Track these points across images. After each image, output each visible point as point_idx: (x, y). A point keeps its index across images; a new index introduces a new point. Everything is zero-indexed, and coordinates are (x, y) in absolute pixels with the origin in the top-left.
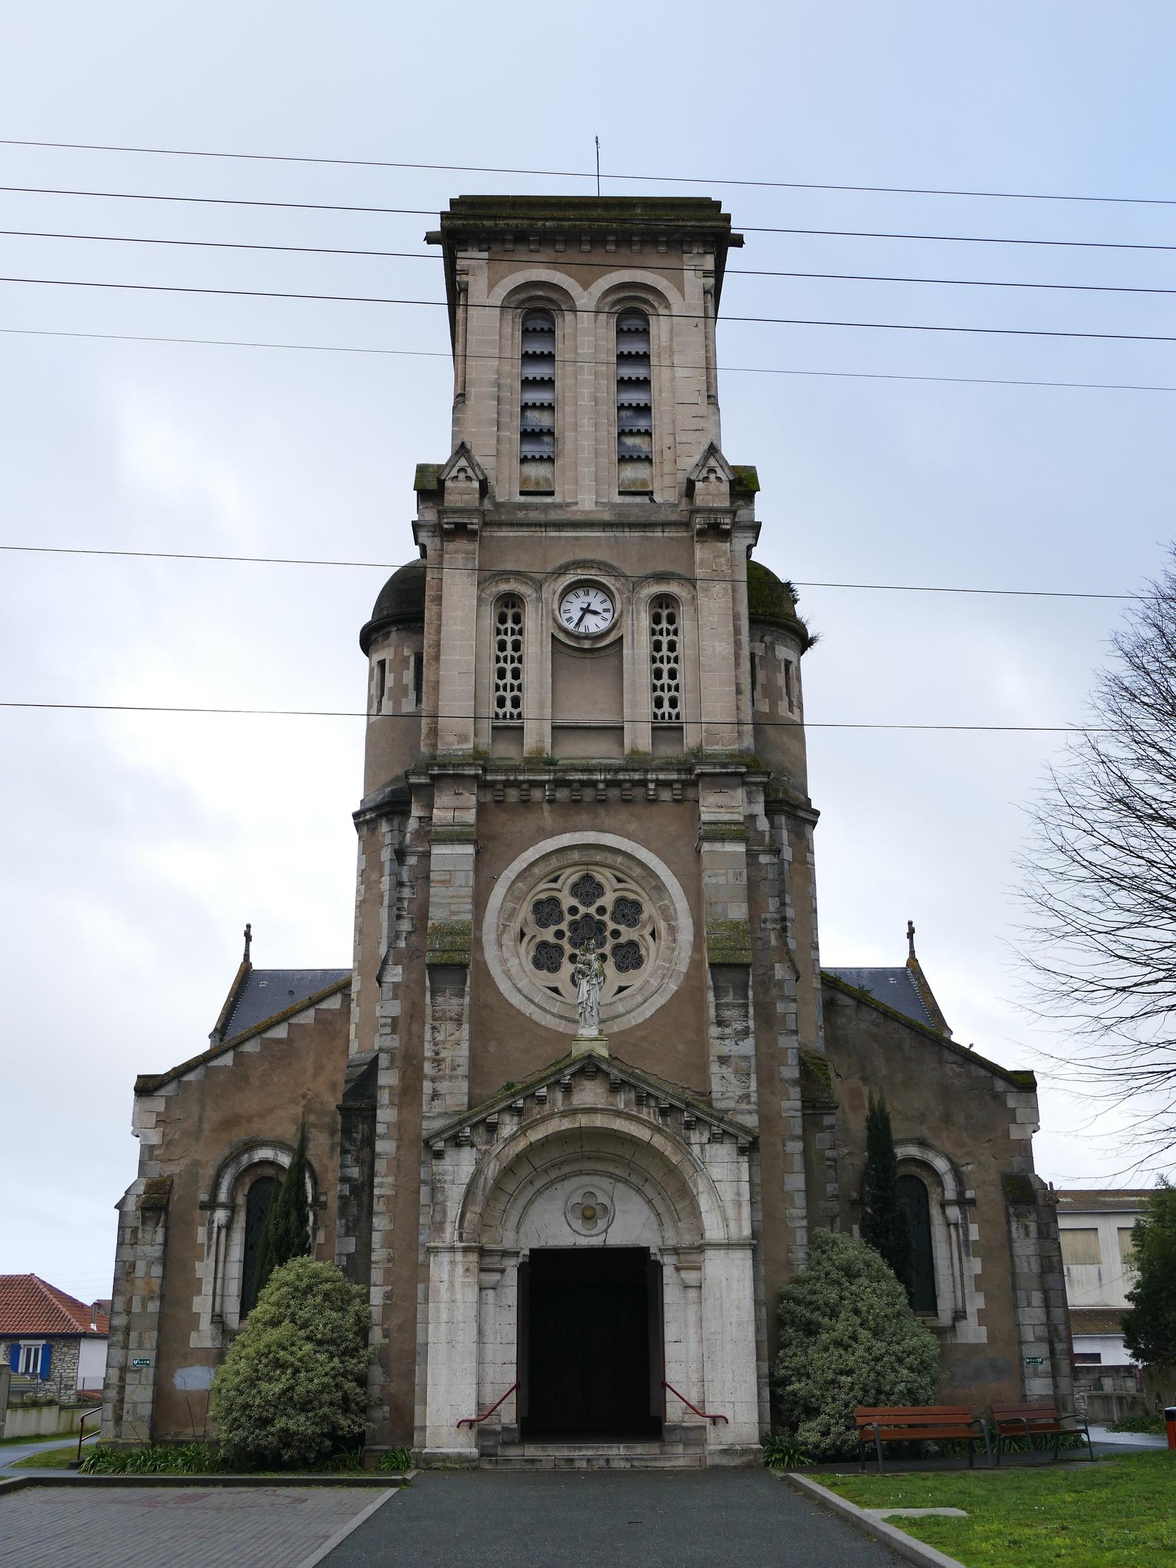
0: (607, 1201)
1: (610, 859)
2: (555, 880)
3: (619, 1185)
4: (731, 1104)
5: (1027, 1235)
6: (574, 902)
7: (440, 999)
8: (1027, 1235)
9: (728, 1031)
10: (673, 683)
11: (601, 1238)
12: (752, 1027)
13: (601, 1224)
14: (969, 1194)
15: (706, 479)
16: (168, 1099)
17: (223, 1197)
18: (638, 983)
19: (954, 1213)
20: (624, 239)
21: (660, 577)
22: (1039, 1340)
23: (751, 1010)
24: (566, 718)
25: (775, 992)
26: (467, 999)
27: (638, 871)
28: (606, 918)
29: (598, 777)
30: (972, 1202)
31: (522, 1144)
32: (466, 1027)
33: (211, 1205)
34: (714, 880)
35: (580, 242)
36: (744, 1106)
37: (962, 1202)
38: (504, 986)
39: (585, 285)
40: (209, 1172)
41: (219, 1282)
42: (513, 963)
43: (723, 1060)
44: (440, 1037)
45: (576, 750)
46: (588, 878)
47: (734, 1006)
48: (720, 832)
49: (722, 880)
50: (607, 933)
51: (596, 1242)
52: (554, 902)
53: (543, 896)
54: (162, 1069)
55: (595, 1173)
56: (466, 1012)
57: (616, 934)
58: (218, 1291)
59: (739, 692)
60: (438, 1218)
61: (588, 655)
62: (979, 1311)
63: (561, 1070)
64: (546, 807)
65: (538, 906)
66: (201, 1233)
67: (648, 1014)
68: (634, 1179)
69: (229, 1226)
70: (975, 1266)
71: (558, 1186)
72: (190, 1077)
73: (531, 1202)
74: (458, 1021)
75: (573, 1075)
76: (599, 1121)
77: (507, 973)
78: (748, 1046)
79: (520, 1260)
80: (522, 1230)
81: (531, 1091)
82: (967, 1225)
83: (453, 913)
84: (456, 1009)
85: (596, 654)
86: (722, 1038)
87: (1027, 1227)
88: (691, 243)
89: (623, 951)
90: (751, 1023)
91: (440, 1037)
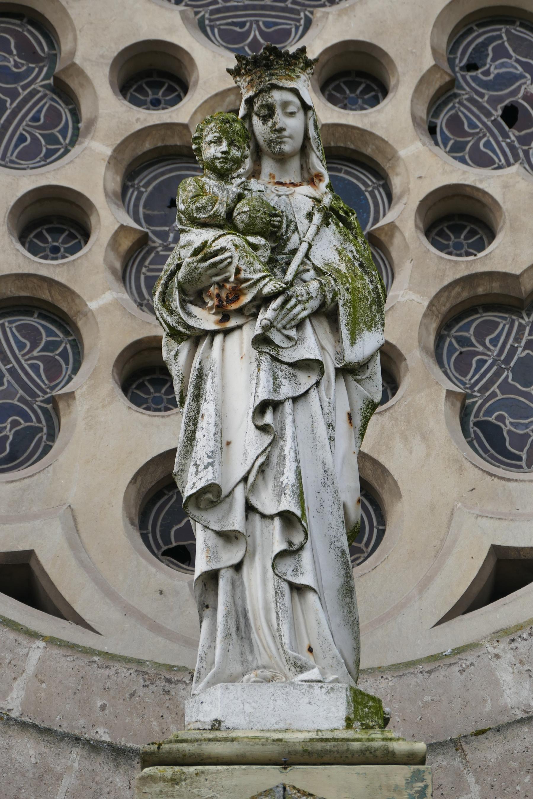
29: (489, 123)
57: (459, 219)
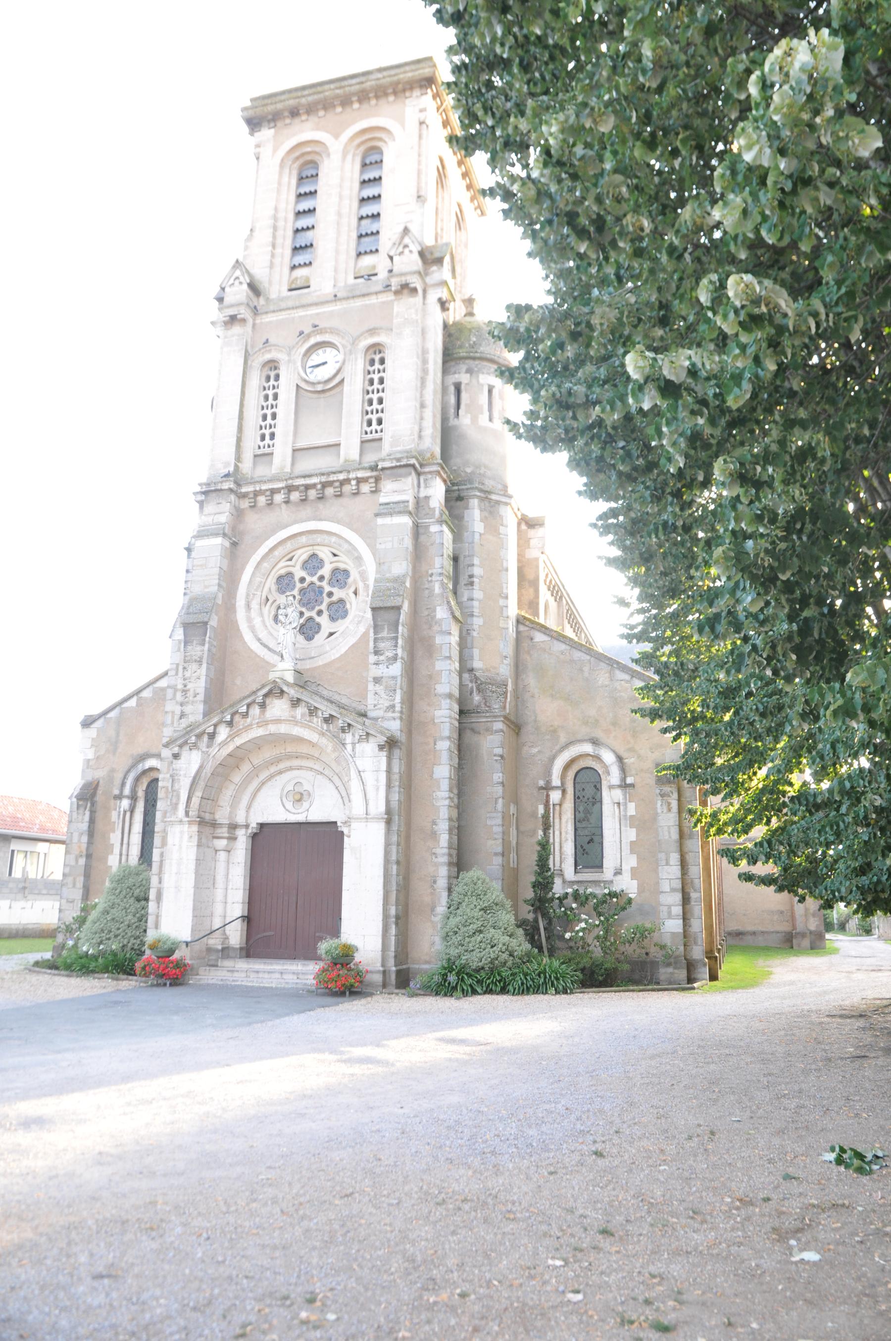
0: (310, 789)
1: (326, 539)
2: (291, 559)
3: (319, 777)
4: (379, 713)
5: (669, 810)
6: (303, 574)
7: (189, 648)
8: (669, 810)
9: (382, 658)
10: (380, 407)
11: (304, 815)
12: (400, 655)
13: (306, 805)
14: (629, 780)
15: (401, 253)
16: (98, 729)
17: (127, 791)
18: (341, 629)
19: (618, 794)
20: (363, 97)
21: (372, 331)
22: (673, 890)
23: (400, 642)
24: (299, 445)
25: (436, 628)
26: (207, 646)
27: (346, 546)
28: (324, 584)
30: (632, 785)
31: (231, 747)
32: (204, 665)
33: (119, 797)
34: (383, 546)
35: (334, 106)
36: (390, 714)
37: (624, 786)
38: (248, 637)
39: (336, 136)
40: (119, 776)
41: (125, 846)
42: (257, 621)
43: (377, 680)
44: (188, 674)
45: (308, 464)
46: (314, 556)
47: (388, 639)
48: (390, 509)
49: (389, 545)
50: (325, 595)
51: (300, 818)
52: (290, 575)
53: (283, 572)
54: (96, 711)
55: (300, 768)
56: (205, 656)
58: (124, 852)
59: (422, 406)
60: (174, 801)
61: (322, 395)
62: (632, 868)
63: (254, 693)
64: (284, 506)
65: (280, 578)
66: (114, 815)
67: (343, 650)
68: (326, 772)
69: (132, 810)
70: (631, 834)
71: (277, 778)
72: (112, 715)
73: (258, 790)
74: (200, 662)
75: (266, 696)
76: (283, 729)
77: (253, 629)
78: (396, 669)
79: (250, 831)
80: (252, 810)
81: (234, 710)
82: (626, 804)
83: (206, 587)
84: (199, 654)
85: (328, 394)
86: (377, 664)
87: (669, 804)
88: (412, 89)
89: (335, 606)
90: (400, 651)
91: (188, 674)
